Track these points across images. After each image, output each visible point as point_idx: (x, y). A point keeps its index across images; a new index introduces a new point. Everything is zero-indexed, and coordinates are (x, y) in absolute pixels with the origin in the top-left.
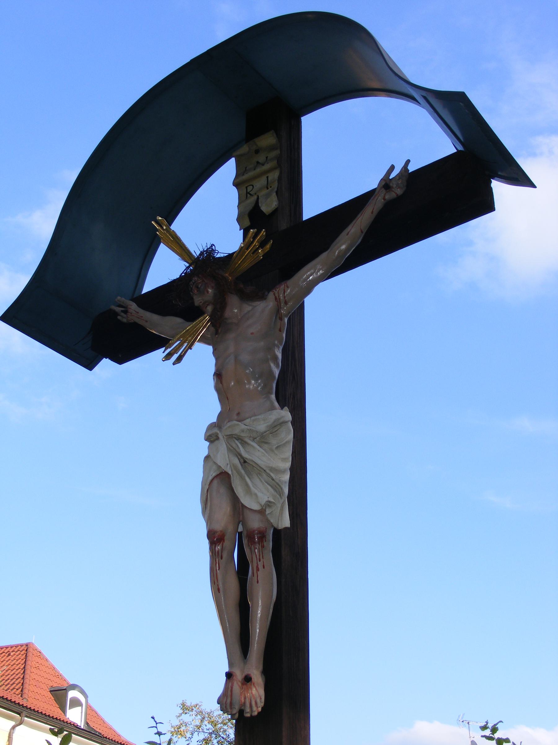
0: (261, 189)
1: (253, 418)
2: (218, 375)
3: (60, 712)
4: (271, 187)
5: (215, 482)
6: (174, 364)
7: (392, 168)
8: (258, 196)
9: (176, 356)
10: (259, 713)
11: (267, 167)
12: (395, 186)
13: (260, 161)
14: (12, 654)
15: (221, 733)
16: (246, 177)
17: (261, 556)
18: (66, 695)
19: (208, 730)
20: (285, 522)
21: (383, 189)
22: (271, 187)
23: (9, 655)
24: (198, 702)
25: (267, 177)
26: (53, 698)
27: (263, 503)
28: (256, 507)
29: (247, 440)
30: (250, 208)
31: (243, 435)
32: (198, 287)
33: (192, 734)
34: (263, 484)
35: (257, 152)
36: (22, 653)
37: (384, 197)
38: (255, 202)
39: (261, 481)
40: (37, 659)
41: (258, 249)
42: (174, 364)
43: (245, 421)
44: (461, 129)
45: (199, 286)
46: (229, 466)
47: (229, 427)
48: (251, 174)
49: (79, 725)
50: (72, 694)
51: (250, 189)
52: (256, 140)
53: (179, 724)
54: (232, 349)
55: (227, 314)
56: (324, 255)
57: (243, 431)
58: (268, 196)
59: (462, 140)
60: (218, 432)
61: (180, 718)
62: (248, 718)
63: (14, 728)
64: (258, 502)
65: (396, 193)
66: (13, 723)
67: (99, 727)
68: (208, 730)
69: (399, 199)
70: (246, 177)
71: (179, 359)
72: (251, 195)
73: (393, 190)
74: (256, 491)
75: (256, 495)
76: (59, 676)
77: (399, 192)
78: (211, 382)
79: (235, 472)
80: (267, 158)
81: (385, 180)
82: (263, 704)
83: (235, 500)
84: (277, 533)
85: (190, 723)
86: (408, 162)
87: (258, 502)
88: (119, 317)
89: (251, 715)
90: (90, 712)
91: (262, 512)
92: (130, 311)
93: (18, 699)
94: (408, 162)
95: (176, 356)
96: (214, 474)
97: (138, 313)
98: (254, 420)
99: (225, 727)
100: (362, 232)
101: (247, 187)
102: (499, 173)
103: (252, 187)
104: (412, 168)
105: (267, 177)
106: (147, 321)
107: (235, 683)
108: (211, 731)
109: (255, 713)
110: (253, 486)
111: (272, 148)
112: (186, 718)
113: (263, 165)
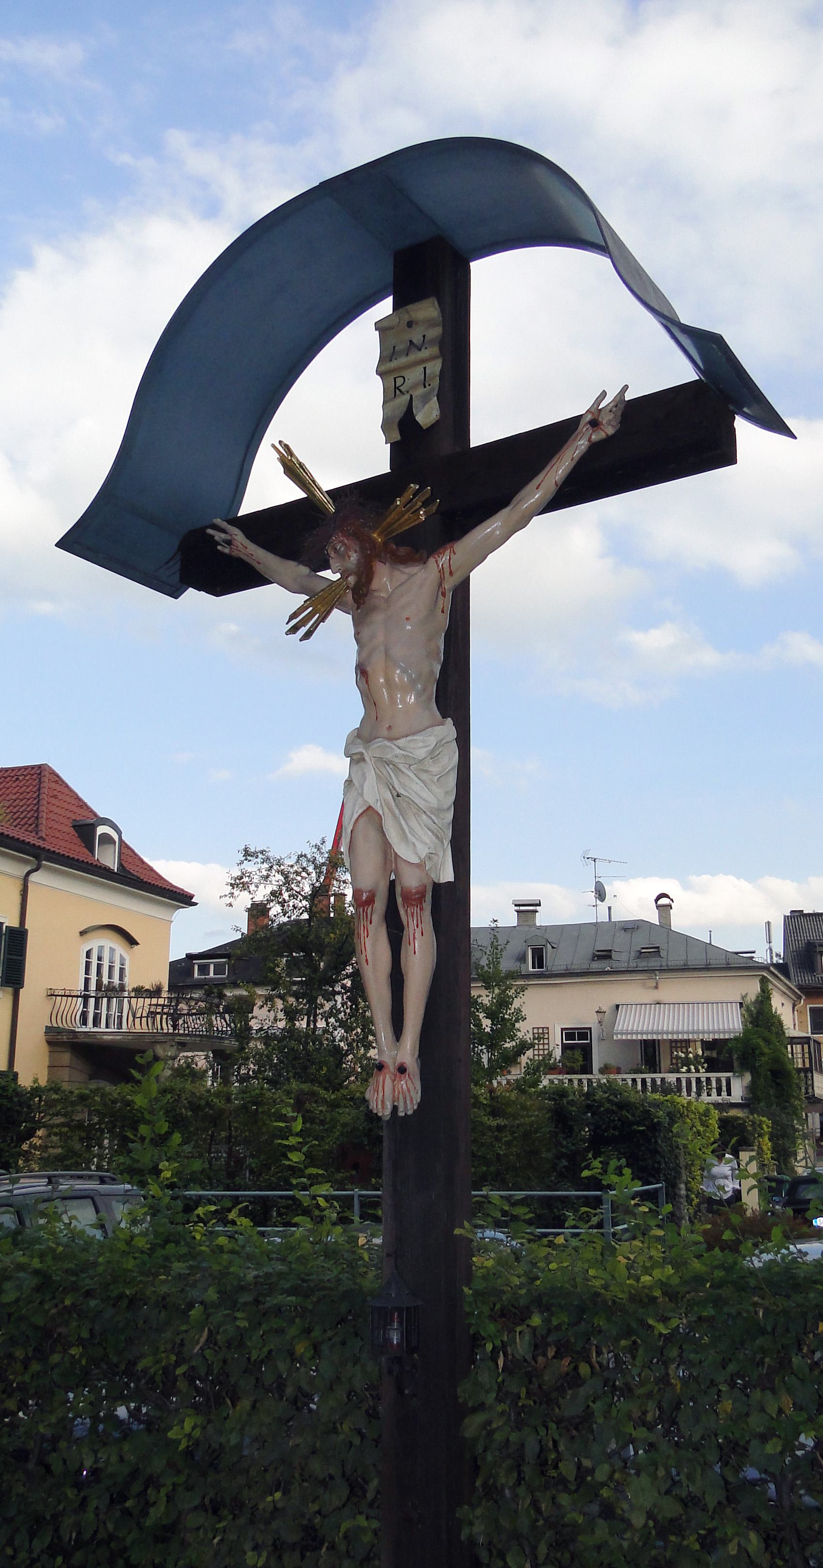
0: (415, 386)
1: (409, 738)
2: (362, 671)
3: (86, 850)
4: (429, 385)
5: (361, 821)
6: (301, 640)
7: (604, 394)
8: (411, 396)
9: (303, 630)
10: (415, 1111)
11: (424, 354)
12: (604, 422)
13: (415, 341)
14: (21, 778)
15: (293, 886)
16: (393, 364)
17: (419, 921)
18: (94, 831)
19: (278, 881)
20: (447, 875)
21: (589, 426)
22: (429, 385)
23: (17, 779)
24: (265, 848)
25: (425, 368)
26: (77, 835)
27: (422, 857)
28: (414, 860)
29: (401, 766)
30: (400, 412)
31: (396, 760)
32: (335, 549)
33: (257, 887)
34: (422, 829)
35: (410, 324)
36: (34, 777)
37: (590, 438)
38: (407, 405)
39: (420, 825)
40: (53, 785)
41: (419, 509)
42: (301, 640)
43: (399, 741)
44: (704, 363)
45: (338, 547)
46: (379, 803)
47: (378, 747)
48: (403, 360)
49: (112, 868)
50: (101, 830)
51: (399, 381)
52: (409, 307)
53: (239, 874)
54: (380, 638)
55: (375, 585)
56: (505, 512)
57: (396, 756)
58: (425, 399)
59: (702, 367)
60: (364, 752)
61: (243, 866)
62: (402, 1117)
63: (28, 874)
64: (417, 854)
65: (606, 433)
66: (28, 868)
67: (137, 869)
68: (278, 881)
69: (609, 439)
70: (393, 364)
71: (308, 635)
72: (400, 391)
73: (602, 427)
74: (414, 840)
75: (414, 844)
76: (83, 805)
77: (610, 431)
78: (351, 676)
79: (386, 809)
80: (424, 337)
81: (593, 413)
82: (419, 1100)
83: (386, 846)
84: (437, 887)
85: (254, 873)
86: (626, 388)
87: (417, 854)
88: (219, 548)
89: (406, 1114)
90: (125, 850)
91: (420, 866)
92: (235, 543)
93: (31, 839)
94: (626, 388)
95: (303, 630)
96: (360, 812)
97: (246, 548)
98: (410, 741)
99: (299, 878)
100: (557, 485)
101: (395, 379)
102: (745, 409)
103: (402, 379)
104: (629, 396)
105: (425, 368)
106: (259, 563)
107: (388, 1076)
108: (281, 883)
109: (410, 1112)
110: (410, 832)
111: (431, 323)
112: (250, 867)
113: (420, 350)
